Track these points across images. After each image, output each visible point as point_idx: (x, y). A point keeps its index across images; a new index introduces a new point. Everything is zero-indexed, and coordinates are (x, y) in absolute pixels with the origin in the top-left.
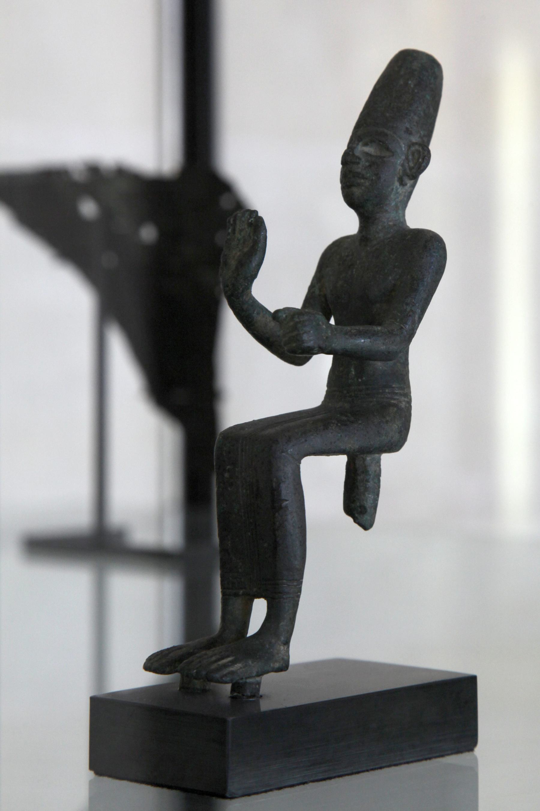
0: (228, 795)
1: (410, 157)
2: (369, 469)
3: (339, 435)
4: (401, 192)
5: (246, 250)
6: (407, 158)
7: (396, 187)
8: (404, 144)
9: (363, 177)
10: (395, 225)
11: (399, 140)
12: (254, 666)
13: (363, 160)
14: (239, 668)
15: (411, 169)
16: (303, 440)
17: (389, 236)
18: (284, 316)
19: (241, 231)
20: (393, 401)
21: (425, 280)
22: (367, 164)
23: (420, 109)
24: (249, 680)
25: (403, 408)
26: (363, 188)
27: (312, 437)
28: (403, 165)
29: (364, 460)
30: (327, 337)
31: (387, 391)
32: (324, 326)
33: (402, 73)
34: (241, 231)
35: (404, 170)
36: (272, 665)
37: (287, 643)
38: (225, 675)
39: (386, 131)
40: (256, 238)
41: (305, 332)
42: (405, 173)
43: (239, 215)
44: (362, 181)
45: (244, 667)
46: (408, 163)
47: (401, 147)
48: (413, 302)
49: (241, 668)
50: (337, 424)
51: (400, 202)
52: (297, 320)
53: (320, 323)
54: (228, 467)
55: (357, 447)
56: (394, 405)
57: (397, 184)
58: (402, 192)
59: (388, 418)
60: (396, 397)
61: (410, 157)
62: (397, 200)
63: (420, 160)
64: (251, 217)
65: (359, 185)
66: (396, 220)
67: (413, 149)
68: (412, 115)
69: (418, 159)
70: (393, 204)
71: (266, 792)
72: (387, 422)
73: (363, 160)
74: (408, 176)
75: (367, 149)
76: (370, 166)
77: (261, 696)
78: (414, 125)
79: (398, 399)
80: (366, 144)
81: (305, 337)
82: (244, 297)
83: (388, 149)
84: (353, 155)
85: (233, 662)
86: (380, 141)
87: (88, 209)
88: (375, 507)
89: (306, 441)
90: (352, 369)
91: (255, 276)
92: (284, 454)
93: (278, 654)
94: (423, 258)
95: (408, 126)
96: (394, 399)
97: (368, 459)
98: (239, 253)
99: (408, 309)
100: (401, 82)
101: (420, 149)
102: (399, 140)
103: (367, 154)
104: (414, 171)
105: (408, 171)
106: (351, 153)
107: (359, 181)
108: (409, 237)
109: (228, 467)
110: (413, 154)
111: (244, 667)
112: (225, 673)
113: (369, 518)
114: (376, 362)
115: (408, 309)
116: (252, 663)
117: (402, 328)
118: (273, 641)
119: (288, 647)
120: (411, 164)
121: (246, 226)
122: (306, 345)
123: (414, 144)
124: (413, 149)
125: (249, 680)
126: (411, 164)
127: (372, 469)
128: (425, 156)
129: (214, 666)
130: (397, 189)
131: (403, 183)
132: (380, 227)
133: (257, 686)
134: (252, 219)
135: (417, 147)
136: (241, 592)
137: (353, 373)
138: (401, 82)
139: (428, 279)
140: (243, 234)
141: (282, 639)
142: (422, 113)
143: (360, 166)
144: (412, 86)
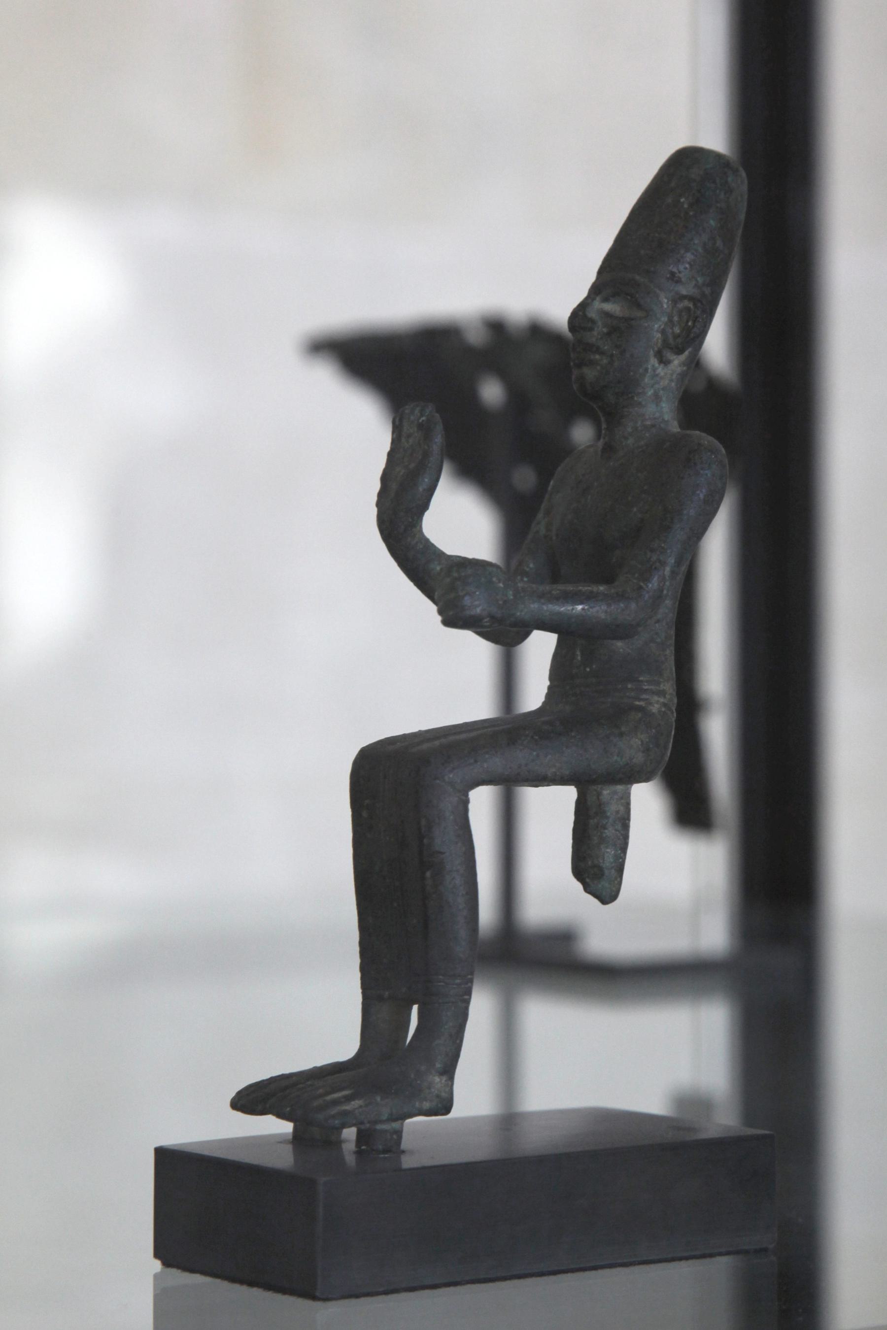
0: (318, 1294)
1: (676, 319)
2: (607, 809)
3: (535, 753)
4: (662, 374)
5: (412, 466)
6: (670, 320)
7: (653, 366)
8: (666, 298)
9: (598, 351)
10: (653, 426)
11: (658, 291)
12: (384, 1106)
13: (600, 323)
14: (356, 1106)
15: (676, 337)
16: (472, 761)
17: (642, 443)
18: (438, 568)
19: (409, 436)
20: (637, 703)
21: (685, 512)
22: (605, 330)
23: (696, 242)
24: (379, 1127)
25: (653, 714)
26: (599, 368)
27: (487, 756)
28: (663, 332)
29: (599, 794)
30: (505, 602)
31: (629, 686)
32: (501, 585)
33: (673, 184)
34: (409, 436)
35: (665, 341)
36: (417, 1104)
37: (449, 1071)
38: (333, 1117)
39: (637, 277)
40: (426, 447)
41: (467, 594)
42: (666, 344)
43: (407, 411)
44: (597, 357)
45: (366, 1106)
46: (672, 328)
47: (661, 303)
48: (663, 548)
49: (361, 1107)
50: (532, 737)
51: (663, 389)
52: (455, 575)
53: (494, 579)
54: (367, 802)
55: (567, 772)
56: (640, 709)
57: (653, 361)
58: (666, 374)
59: (623, 729)
60: (644, 696)
61: (676, 319)
62: (657, 386)
63: (690, 324)
64: (422, 415)
65: (592, 363)
66: (655, 418)
67: (680, 305)
68: (682, 252)
69: (687, 322)
70: (650, 393)
71: (386, 1293)
72: (621, 735)
73: (600, 323)
74: (671, 349)
75: (608, 307)
76: (609, 334)
77: (403, 1152)
78: (686, 268)
79: (647, 699)
80: (606, 300)
81: (467, 601)
82: (409, 539)
83: (639, 306)
84: (585, 316)
85: (348, 1099)
86: (627, 294)
87: (492, 392)
88: (620, 869)
89: (476, 761)
90: (578, 653)
91: (425, 506)
92: (438, 781)
93: (429, 1088)
94: (682, 478)
95: (675, 270)
96: (640, 700)
97: (605, 792)
98: (403, 471)
99: (654, 558)
100: (669, 200)
101: (691, 305)
102: (658, 291)
103: (607, 315)
104: (679, 340)
105: (671, 341)
106: (581, 313)
107: (592, 357)
108: (668, 444)
109: (367, 802)
110: (680, 312)
111: (366, 1106)
112: (333, 1113)
113: (607, 885)
114: (614, 642)
115: (654, 558)
116: (382, 1099)
117: (641, 588)
118: (423, 1068)
119: (451, 1078)
120: (677, 330)
121: (416, 429)
122: (468, 613)
123: (683, 298)
124: (680, 305)
125: (379, 1127)
126: (677, 330)
127: (613, 808)
128: (697, 318)
129: (316, 1103)
130: (654, 370)
131: (664, 359)
132: (630, 430)
133: (395, 1137)
134: (424, 418)
135: (686, 303)
136: (387, 994)
137: (579, 658)
138: (669, 200)
139: (691, 511)
140: (411, 441)
141: (438, 1065)
142: (700, 250)
143: (595, 333)
144: (686, 206)
